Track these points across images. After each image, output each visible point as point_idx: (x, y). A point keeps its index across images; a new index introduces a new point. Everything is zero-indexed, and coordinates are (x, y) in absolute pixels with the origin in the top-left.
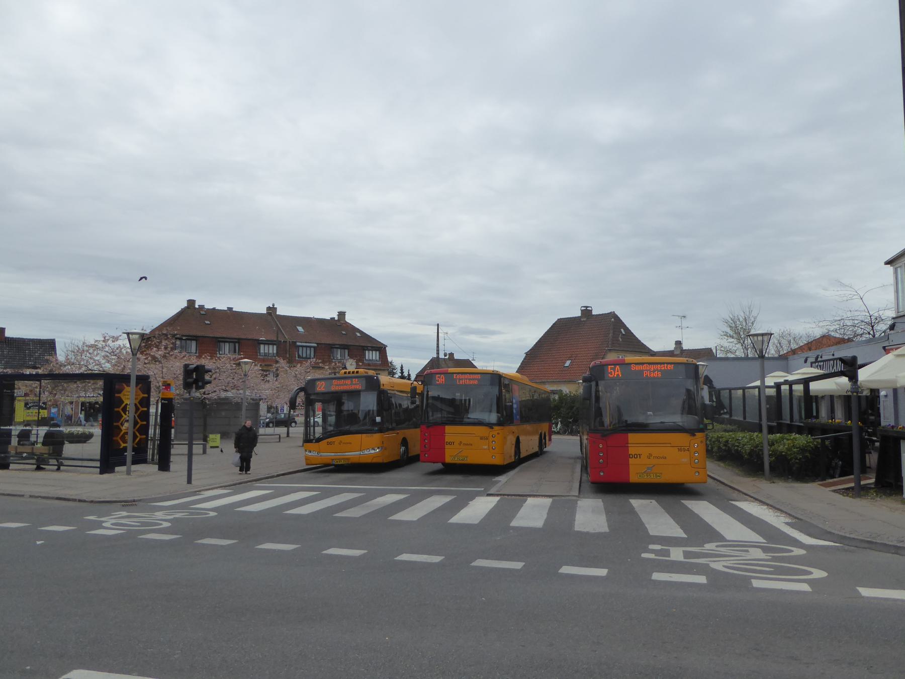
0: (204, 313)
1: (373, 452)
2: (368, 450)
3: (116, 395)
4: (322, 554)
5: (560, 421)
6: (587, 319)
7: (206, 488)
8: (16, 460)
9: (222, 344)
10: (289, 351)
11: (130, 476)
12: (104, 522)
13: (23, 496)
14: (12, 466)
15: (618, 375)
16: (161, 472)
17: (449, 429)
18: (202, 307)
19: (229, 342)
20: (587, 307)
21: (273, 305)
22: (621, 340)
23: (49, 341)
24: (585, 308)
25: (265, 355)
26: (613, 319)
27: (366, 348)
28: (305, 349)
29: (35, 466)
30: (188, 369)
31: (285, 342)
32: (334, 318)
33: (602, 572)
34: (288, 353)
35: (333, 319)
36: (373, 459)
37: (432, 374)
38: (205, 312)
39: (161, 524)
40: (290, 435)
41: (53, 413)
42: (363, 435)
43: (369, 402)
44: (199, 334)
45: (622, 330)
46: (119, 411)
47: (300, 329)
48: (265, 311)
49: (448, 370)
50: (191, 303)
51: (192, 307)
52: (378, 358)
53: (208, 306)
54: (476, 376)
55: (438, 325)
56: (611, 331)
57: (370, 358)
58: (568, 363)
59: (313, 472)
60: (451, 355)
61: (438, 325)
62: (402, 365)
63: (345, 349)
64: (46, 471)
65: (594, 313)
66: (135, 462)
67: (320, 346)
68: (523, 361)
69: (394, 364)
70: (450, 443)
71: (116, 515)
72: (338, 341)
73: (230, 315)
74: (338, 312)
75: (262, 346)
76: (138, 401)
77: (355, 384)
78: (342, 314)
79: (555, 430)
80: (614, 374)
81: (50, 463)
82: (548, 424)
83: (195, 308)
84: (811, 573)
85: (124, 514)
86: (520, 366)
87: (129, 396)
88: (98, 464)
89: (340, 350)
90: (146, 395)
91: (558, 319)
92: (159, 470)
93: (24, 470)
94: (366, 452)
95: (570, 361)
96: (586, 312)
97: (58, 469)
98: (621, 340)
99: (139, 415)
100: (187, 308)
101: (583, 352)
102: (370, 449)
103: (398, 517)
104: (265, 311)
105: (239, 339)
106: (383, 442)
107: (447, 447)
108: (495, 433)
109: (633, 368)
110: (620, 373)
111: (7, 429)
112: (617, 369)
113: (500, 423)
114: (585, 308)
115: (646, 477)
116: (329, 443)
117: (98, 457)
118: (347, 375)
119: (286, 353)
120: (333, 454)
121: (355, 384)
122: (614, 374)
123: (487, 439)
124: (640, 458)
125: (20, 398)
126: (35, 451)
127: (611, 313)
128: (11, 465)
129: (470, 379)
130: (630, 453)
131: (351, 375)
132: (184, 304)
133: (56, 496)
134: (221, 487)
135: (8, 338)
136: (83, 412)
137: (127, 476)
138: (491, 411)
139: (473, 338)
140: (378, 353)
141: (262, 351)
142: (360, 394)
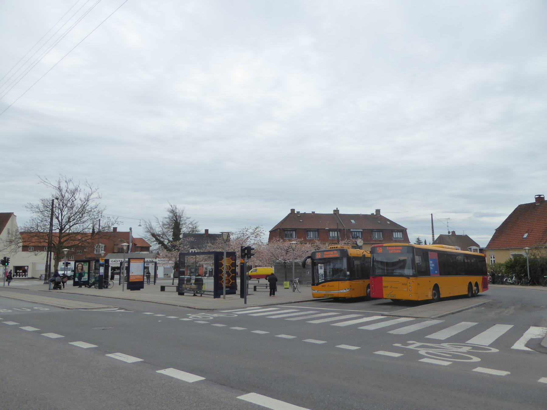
0: (299, 216)
1: (345, 291)
2: (343, 290)
3: (220, 261)
5: (515, 275)
6: (541, 203)
7: (255, 305)
8: (187, 291)
9: (309, 233)
10: (347, 235)
11: (224, 300)
13: (177, 306)
14: (185, 294)
16: (241, 298)
17: (384, 278)
18: (298, 213)
19: (313, 231)
20: (540, 195)
21: (337, 209)
23: (524, 205)
24: (538, 196)
25: (333, 237)
27: (393, 231)
28: (358, 233)
29: (193, 294)
30: (242, 248)
31: (344, 229)
32: (374, 214)
35: (373, 214)
36: (345, 295)
37: (375, 247)
38: (300, 215)
39: (210, 318)
43: (344, 264)
44: (297, 228)
46: (221, 269)
47: (353, 221)
48: (332, 213)
49: (383, 245)
50: (293, 211)
52: (401, 237)
53: (302, 212)
54: (399, 248)
55: (432, 214)
57: (397, 237)
58: (525, 236)
59: (317, 302)
60: (453, 232)
61: (432, 214)
62: (425, 240)
63: (380, 232)
66: (228, 293)
67: (365, 231)
68: (494, 235)
69: (420, 240)
70: (386, 287)
72: (376, 227)
73: (314, 216)
74: (376, 210)
75: (331, 233)
76: (230, 264)
77: (335, 254)
78: (378, 211)
79: (511, 281)
81: (205, 294)
82: (482, 277)
84: (472, 359)
85: (203, 314)
86: (492, 239)
87: (226, 262)
88: (213, 294)
90: (234, 262)
91: (519, 205)
92: (241, 297)
93: (189, 296)
94: (341, 291)
95: (527, 234)
97: (201, 296)
99: (231, 271)
102: (344, 290)
103: (391, 332)
104: (332, 213)
105: (318, 229)
106: (351, 286)
111: (182, 277)
113: (414, 276)
114: (538, 196)
116: (323, 286)
117: (213, 291)
118: (332, 249)
119: (345, 236)
120: (325, 292)
121: (335, 254)
123: (406, 285)
128: (185, 293)
129: (396, 250)
131: (334, 249)
134: (288, 303)
135: (210, 234)
137: (223, 300)
138: (410, 269)
139: (485, 219)
140: (401, 233)
141: (331, 235)
142: (343, 259)
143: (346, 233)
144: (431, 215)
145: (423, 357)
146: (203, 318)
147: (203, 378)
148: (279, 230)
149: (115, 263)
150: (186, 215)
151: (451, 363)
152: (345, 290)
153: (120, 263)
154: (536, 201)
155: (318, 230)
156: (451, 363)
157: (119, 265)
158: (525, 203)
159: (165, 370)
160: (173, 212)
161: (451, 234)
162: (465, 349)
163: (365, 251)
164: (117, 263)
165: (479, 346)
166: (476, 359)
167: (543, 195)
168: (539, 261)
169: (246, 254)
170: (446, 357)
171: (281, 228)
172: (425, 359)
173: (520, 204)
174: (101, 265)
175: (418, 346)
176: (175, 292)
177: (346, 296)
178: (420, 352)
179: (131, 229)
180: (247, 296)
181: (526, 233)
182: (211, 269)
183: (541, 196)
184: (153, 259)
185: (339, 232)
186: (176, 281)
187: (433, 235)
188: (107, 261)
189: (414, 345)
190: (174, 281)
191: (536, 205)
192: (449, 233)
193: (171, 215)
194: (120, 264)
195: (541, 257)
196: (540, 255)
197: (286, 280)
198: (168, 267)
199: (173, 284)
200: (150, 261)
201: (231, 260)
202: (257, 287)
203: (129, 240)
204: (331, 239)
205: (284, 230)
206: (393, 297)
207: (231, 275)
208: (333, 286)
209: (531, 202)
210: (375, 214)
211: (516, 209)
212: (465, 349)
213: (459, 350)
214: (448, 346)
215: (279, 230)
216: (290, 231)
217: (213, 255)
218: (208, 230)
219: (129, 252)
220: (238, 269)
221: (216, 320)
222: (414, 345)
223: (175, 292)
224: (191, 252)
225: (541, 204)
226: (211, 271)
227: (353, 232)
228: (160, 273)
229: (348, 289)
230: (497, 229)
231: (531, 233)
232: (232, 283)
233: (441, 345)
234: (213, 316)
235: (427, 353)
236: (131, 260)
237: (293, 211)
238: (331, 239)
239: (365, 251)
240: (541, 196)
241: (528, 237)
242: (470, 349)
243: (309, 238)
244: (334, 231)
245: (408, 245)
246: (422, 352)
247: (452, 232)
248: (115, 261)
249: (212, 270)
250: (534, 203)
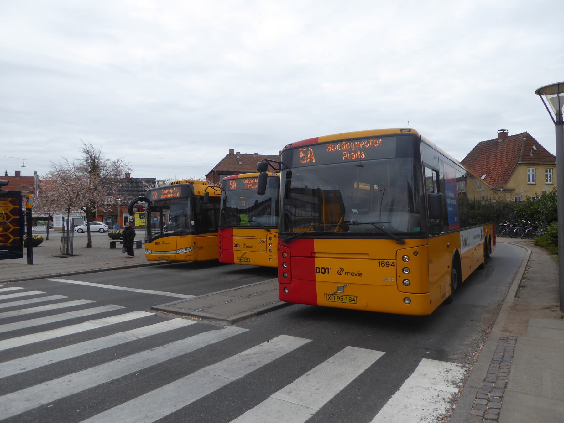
0: (239, 157)
6: (504, 140)
15: (311, 160)
16: (28, 265)
18: (238, 153)
22: (532, 155)
24: (501, 131)
40: (49, 238)
41: (154, 221)
42: (178, 236)
45: (534, 147)
49: (237, 176)
50: (231, 151)
51: (232, 154)
53: (242, 152)
56: (523, 148)
59: (154, 267)
65: (509, 134)
80: (307, 160)
83: (234, 155)
90: (18, 207)
91: (480, 143)
95: (485, 175)
96: (503, 134)
98: (532, 155)
107: (235, 248)
108: (271, 235)
109: (329, 149)
110: (313, 157)
112: (309, 152)
114: (501, 131)
115: (336, 300)
122: (307, 160)
123: (265, 241)
124: (328, 273)
125: (136, 213)
127: (524, 133)
130: (316, 266)
131: (176, 184)
132: (228, 152)
134: (68, 275)
136: (171, 220)
150: (104, 156)
152: (186, 249)
154: (498, 137)
158: (486, 140)
160: (87, 152)
163: (211, 187)
167: (507, 130)
168: (495, 205)
171: (215, 171)
173: (480, 142)
177: (188, 258)
181: (484, 174)
182: (132, 219)
183: (504, 131)
191: (498, 142)
193: (85, 156)
195: (497, 201)
196: (497, 198)
198: (77, 217)
201: (10, 204)
202: (116, 242)
206: (246, 261)
207: (10, 228)
208: (169, 243)
209: (493, 139)
211: (476, 147)
220: (164, 218)
225: (504, 141)
226: (133, 221)
229: (190, 248)
231: (489, 173)
232: (12, 241)
237: (231, 151)
239: (211, 187)
240: (504, 131)
241: (486, 178)
245: (272, 175)
249: (133, 220)
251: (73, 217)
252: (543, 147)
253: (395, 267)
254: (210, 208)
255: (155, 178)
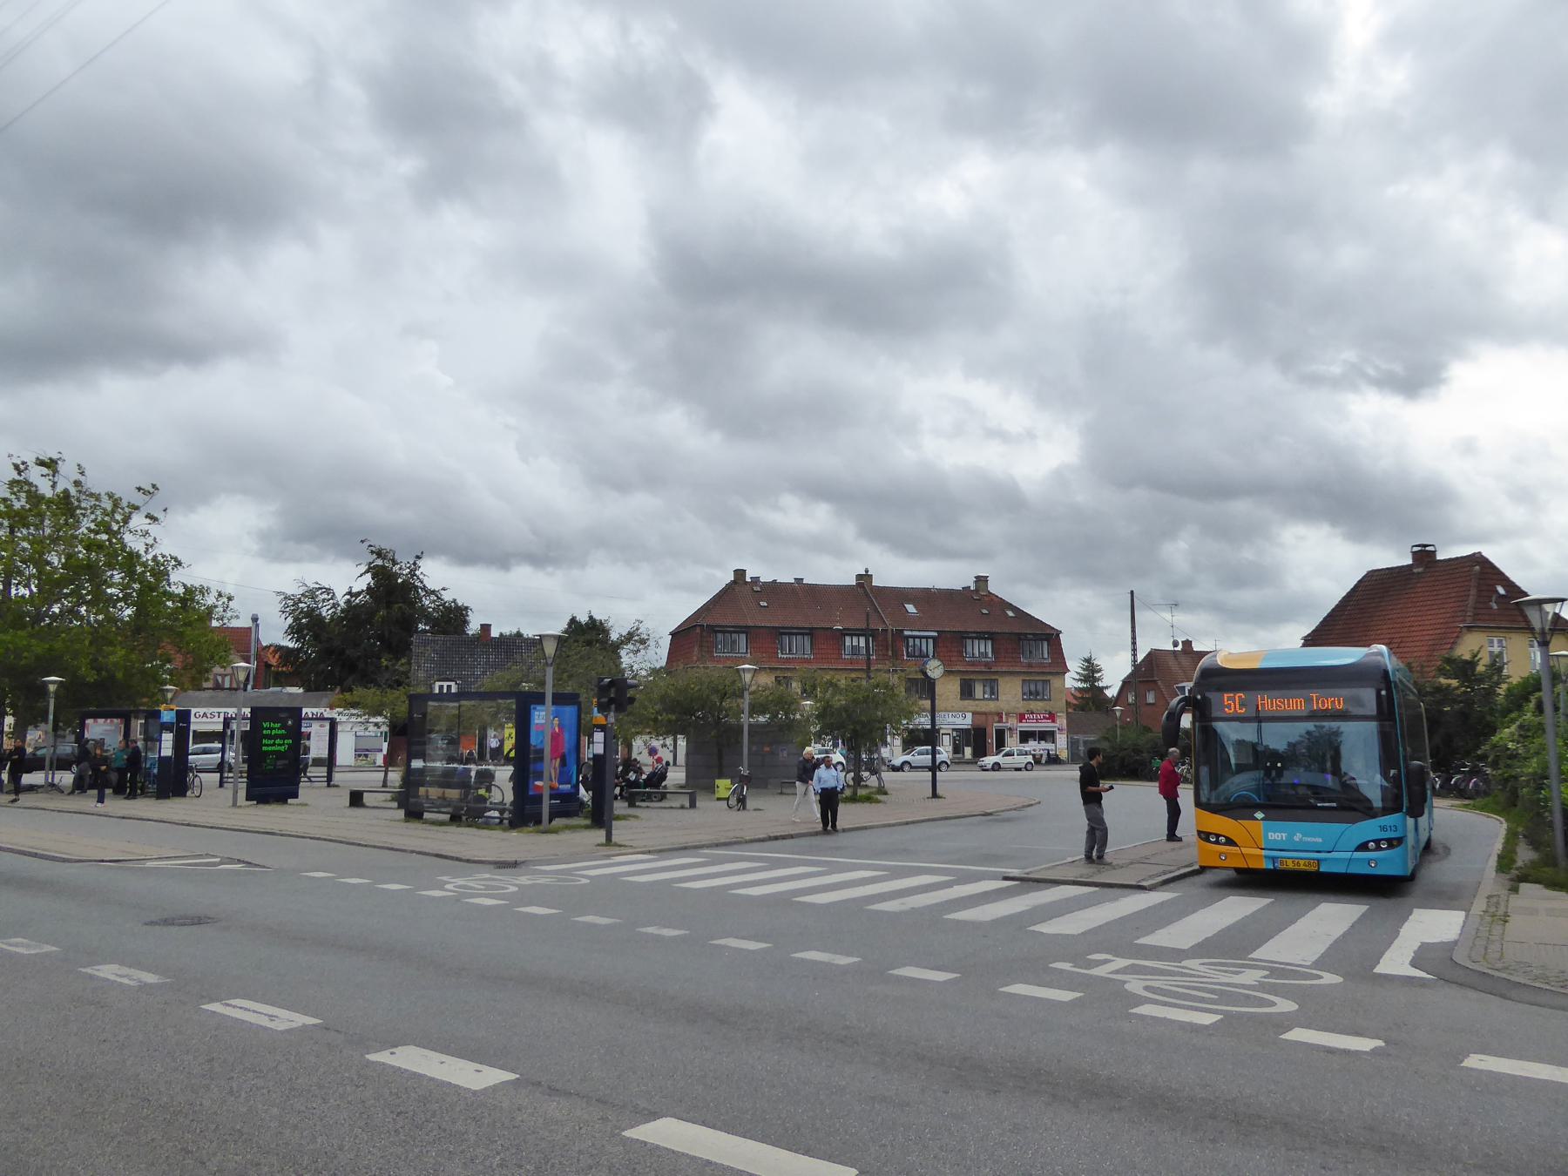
4: (791, 957)
12: (1125, 982)
14: (426, 815)
18: (755, 580)
21: (867, 571)
22: (1495, 607)
24: (1419, 548)
26: (1477, 567)
30: (602, 683)
33: (1474, 1061)
34: (890, 649)
35: (967, 589)
38: (761, 587)
47: (911, 608)
50: (740, 574)
51: (741, 582)
55: (1132, 592)
56: (1473, 592)
60: (1187, 644)
64: (288, 806)
65: (1440, 557)
69: (1095, 662)
71: (1175, 966)
75: (848, 639)
84: (1273, 1004)
85: (488, 876)
89: (984, 641)
91: (1369, 573)
98: (1495, 607)
100: (734, 582)
101: (1427, 638)
103: (1049, 928)
114: (1419, 548)
119: (887, 650)
126: (446, 796)
133: (435, 852)
143: (890, 642)
144: (1130, 595)
145: (1140, 1001)
146: (488, 888)
147: (512, 1076)
148: (698, 630)
149: (204, 719)
151: (1220, 1017)
153: (222, 719)
155: (811, 633)
156: (1220, 1017)
157: (220, 728)
159: (392, 1053)
161: (1179, 648)
162: (1251, 977)
164: (212, 720)
165: (1298, 969)
166: (1285, 1006)
169: (611, 701)
170: (1202, 1000)
172: (1146, 1006)
174: (167, 727)
175: (1097, 966)
176: (816, 834)
178: (1127, 986)
179: (255, 619)
180: (614, 823)
183: (1427, 548)
184: (322, 710)
185: (871, 639)
186: (395, 776)
187: (1134, 650)
188: (184, 716)
189: (1110, 966)
190: (390, 774)
192: (1175, 644)
194: (224, 722)
197: (721, 776)
199: (385, 785)
200: (313, 714)
203: (249, 651)
204: (849, 657)
205: (713, 630)
210: (972, 588)
212: (1251, 977)
213: (1237, 979)
214: (1202, 968)
215: (698, 630)
216: (731, 632)
217: (514, 701)
218: (247, 800)
219: (249, 687)
221: (527, 896)
222: (1110, 966)
223: (816, 834)
224: (437, 691)
225: (1428, 570)
227: (911, 640)
228: (345, 753)
230: (1309, 635)
233: (1184, 963)
234: (518, 882)
235: (1147, 988)
236: (576, 707)
237: (740, 574)
238: (849, 657)
240: (1427, 548)
242: (1265, 977)
243: (786, 654)
244: (858, 635)
246: (1135, 985)
247: (1183, 642)
248: (205, 715)
250: (1408, 566)
251: (358, 734)
252: (1519, 588)
253: (1085, 871)
254: (52, 751)
255: (573, 621)
